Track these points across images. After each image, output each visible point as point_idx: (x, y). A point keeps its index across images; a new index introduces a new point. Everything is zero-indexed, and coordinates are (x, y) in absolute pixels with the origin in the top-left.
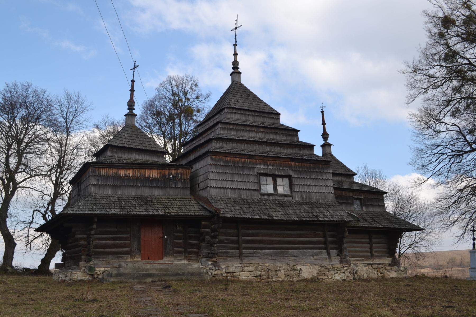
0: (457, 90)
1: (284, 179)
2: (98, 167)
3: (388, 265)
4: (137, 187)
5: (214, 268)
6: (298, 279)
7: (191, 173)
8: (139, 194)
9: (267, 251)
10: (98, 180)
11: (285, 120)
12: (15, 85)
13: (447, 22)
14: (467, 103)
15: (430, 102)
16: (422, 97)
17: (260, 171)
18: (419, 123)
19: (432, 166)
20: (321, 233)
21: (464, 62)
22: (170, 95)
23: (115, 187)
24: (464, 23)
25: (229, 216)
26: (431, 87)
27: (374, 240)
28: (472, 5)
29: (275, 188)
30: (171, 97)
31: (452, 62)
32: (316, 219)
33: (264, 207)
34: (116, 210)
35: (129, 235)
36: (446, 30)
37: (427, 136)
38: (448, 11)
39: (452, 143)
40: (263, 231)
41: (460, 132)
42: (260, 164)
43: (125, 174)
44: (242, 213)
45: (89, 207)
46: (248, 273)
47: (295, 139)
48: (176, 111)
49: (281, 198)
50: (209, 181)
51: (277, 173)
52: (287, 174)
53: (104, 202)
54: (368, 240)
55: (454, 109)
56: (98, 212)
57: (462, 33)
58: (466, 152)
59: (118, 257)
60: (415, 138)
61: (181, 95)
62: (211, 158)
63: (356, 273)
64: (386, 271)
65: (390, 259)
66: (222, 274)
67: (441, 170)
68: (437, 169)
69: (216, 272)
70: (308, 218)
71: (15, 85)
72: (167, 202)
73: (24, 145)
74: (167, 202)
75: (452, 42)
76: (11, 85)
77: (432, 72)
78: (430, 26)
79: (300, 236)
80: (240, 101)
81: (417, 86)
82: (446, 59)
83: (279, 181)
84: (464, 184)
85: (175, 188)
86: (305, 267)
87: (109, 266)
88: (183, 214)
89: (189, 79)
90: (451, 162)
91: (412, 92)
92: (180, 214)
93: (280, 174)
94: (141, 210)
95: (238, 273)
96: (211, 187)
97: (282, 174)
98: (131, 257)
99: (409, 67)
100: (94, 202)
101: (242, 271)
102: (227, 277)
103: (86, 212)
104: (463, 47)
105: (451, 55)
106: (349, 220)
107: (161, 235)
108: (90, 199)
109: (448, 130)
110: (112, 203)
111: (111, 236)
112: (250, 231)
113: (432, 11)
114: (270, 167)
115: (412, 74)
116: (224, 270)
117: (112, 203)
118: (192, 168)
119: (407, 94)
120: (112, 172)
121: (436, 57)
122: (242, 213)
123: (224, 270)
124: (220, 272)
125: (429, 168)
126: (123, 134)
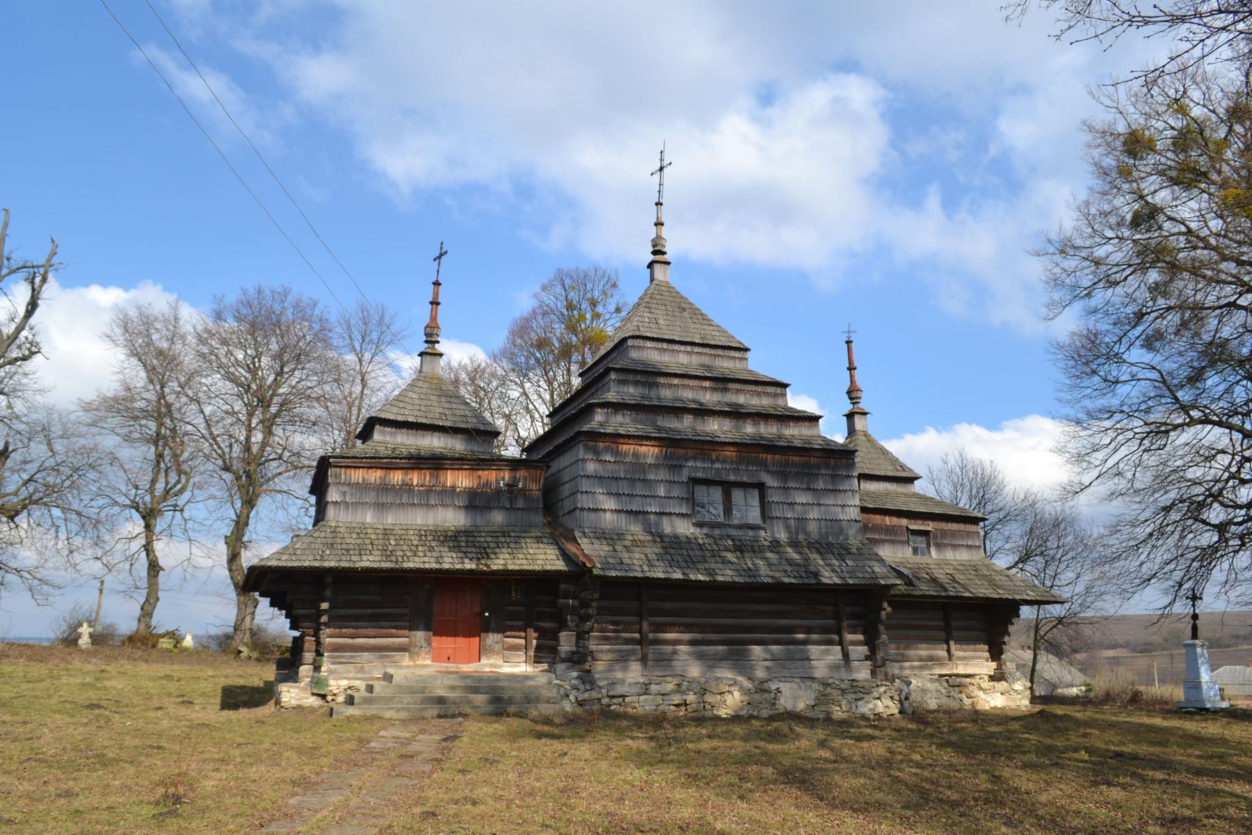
0: (1157, 290)
1: (751, 490)
2: (347, 467)
3: (986, 678)
4: (428, 506)
5: (582, 687)
6: (771, 712)
7: (546, 479)
8: (431, 522)
9: (705, 648)
10: (344, 493)
11: (759, 364)
12: (260, 292)
13: (1136, 144)
14: (1182, 319)
15: (1100, 316)
16: (1078, 306)
17: (693, 475)
18: (1072, 363)
19: (1100, 456)
20: (829, 608)
21: (1176, 230)
22: (561, 306)
23: (381, 507)
24: (1174, 144)
25: (411, 565)
26: (1101, 284)
27: (954, 624)
28: (1192, 104)
29: (728, 511)
30: (564, 311)
31: (1148, 231)
32: (813, 581)
33: (698, 553)
34: (371, 558)
35: (406, 611)
36: (1132, 161)
37: (1089, 391)
38: (1137, 120)
39: (1143, 407)
40: (696, 605)
41: (1164, 382)
42: (695, 458)
43: (403, 481)
44: (646, 569)
45: (315, 552)
46: (659, 699)
47: (780, 402)
48: (574, 338)
49: (741, 533)
50: (579, 495)
51: (732, 478)
52: (754, 480)
53: (352, 540)
54: (941, 623)
55: (1150, 332)
56: (332, 564)
57: (1170, 168)
58: (1176, 427)
59: (381, 657)
60: (1062, 395)
61: (585, 305)
62: (586, 447)
63: (907, 699)
64: (981, 694)
65: (994, 665)
66: (599, 700)
67: (1121, 465)
68: (1110, 463)
69: (586, 695)
70: (795, 577)
71: (260, 292)
72: (489, 539)
73: (273, 409)
74: (489, 539)
75: (1150, 184)
76: (251, 291)
77: (1100, 252)
78: (1096, 153)
79: (781, 615)
80: (661, 322)
81: (1068, 281)
82: (1136, 222)
83: (737, 495)
84: (1173, 495)
85: (512, 508)
86: (788, 685)
87: (360, 675)
88: (517, 568)
89: (600, 273)
90: (1143, 448)
91: (1056, 296)
92: (510, 567)
93: (739, 479)
94: (426, 559)
95: (635, 698)
96: (582, 509)
97: (745, 479)
98: (411, 658)
99: (1050, 242)
100: (330, 541)
101: (645, 694)
102: (609, 706)
103: (306, 564)
104: (1170, 197)
105: (1147, 216)
106: (890, 582)
107: (477, 609)
108: (323, 535)
109: (1134, 378)
110: (367, 541)
111: (369, 611)
112: (668, 605)
113: (1103, 121)
114: (717, 465)
115: (1058, 258)
116: (604, 691)
117: (367, 541)
118: (548, 467)
119: (1045, 299)
120: (375, 476)
121: (1113, 220)
122: (646, 569)
123: (604, 691)
124: (594, 694)
125: (1092, 460)
126: (410, 394)
